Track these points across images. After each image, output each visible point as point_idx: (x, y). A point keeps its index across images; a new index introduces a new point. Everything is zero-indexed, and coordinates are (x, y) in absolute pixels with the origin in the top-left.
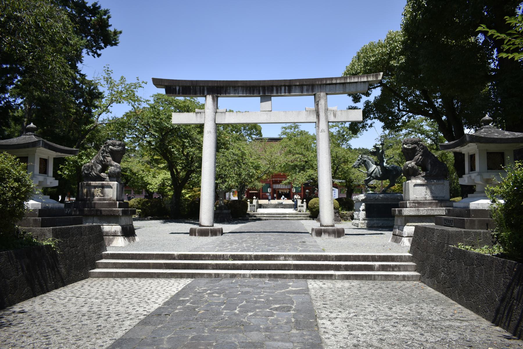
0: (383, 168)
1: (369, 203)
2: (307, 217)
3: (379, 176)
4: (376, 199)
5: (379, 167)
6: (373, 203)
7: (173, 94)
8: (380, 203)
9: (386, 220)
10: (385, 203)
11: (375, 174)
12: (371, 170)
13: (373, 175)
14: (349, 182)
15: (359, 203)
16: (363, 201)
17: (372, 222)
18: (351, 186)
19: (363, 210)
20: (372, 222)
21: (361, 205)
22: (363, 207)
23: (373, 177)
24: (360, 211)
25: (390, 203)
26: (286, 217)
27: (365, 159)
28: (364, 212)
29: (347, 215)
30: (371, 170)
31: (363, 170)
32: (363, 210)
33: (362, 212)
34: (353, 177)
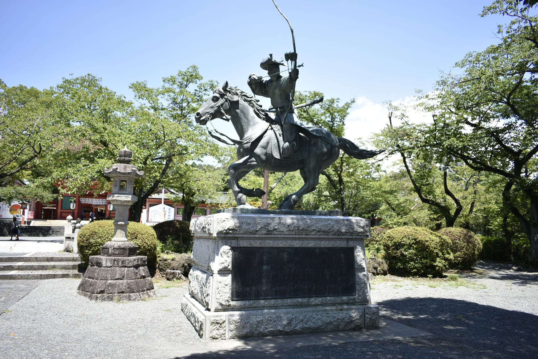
0: (292, 131)
1: (244, 244)
2: (74, 267)
3: (277, 155)
4: (269, 232)
5: (277, 127)
6: (257, 244)
7: (335, 293)
8: (281, 244)
9: (301, 306)
10: (297, 244)
11: (265, 147)
12: (252, 134)
13: (258, 150)
14: (187, 194)
15: (210, 243)
16: (225, 236)
17: (256, 317)
18: (192, 202)
19: (223, 272)
20: (256, 317)
21: (216, 251)
22: (224, 258)
23: (257, 157)
24: (208, 272)
25: (312, 244)
26: (11, 268)
27: (236, 98)
28: (228, 279)
29: (174, 264)
30: (252, 134)
31: (225, 127)
32: (223, 272)
33: (216, 276)
34: (194, 187)
